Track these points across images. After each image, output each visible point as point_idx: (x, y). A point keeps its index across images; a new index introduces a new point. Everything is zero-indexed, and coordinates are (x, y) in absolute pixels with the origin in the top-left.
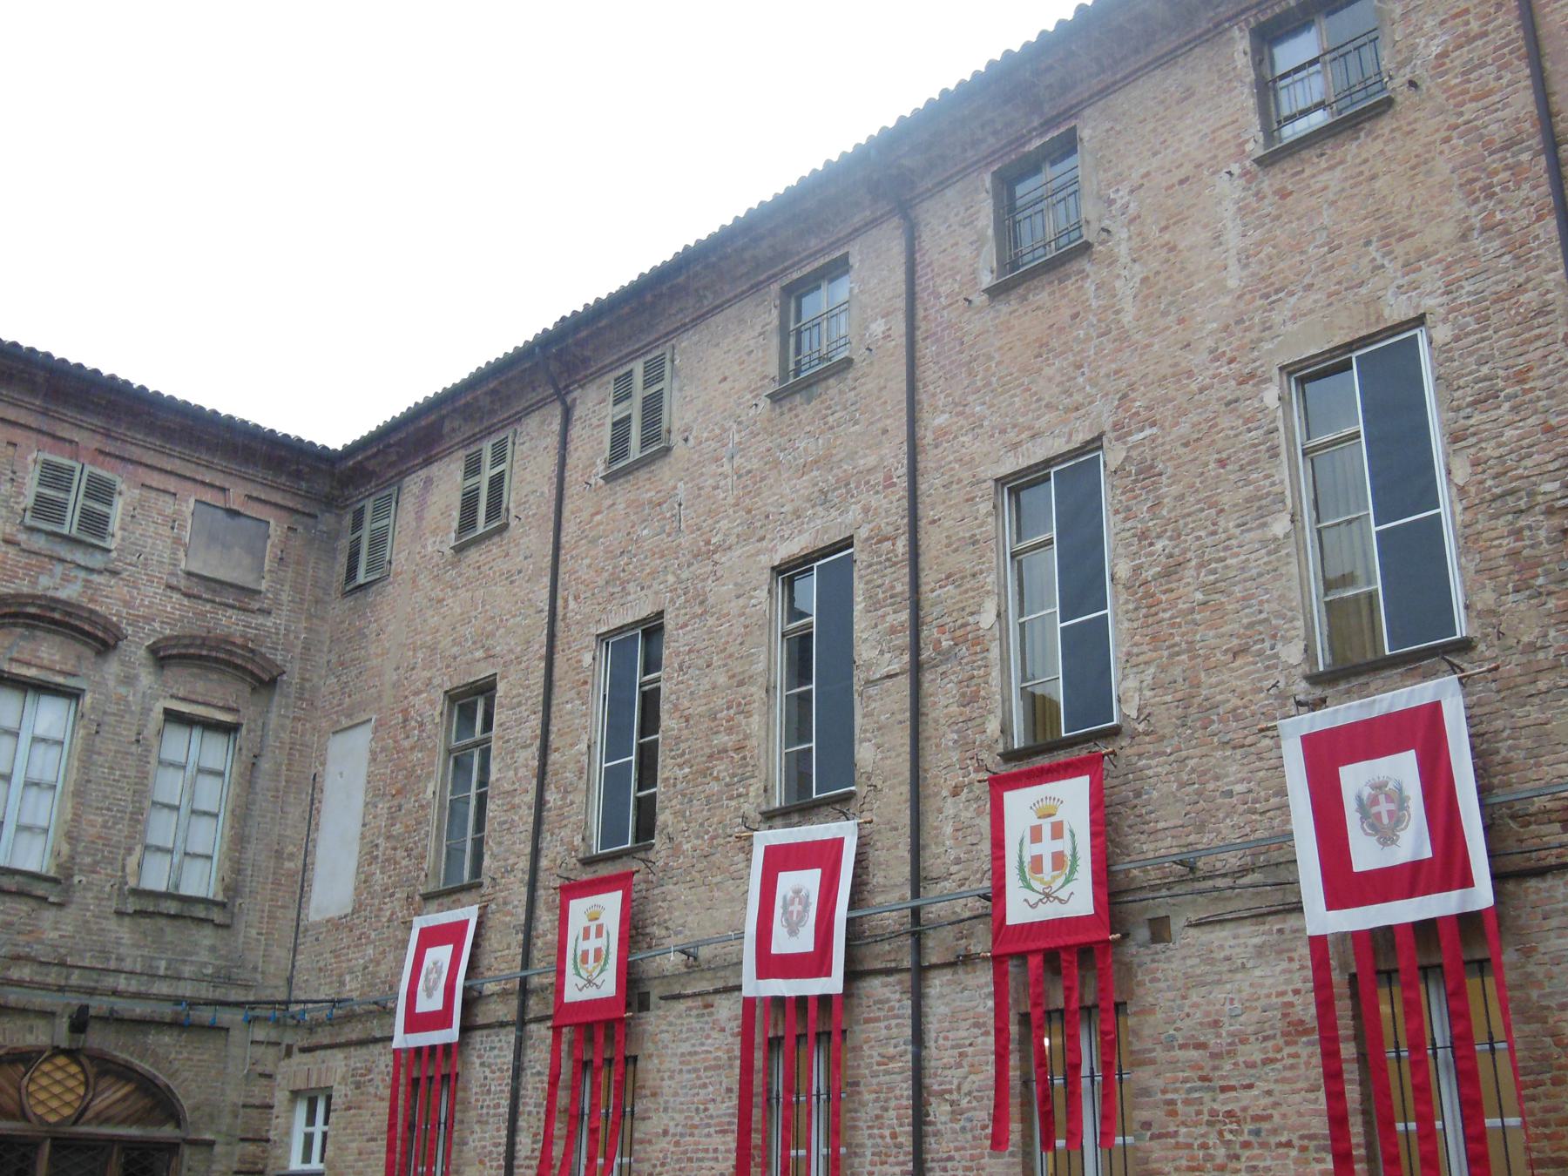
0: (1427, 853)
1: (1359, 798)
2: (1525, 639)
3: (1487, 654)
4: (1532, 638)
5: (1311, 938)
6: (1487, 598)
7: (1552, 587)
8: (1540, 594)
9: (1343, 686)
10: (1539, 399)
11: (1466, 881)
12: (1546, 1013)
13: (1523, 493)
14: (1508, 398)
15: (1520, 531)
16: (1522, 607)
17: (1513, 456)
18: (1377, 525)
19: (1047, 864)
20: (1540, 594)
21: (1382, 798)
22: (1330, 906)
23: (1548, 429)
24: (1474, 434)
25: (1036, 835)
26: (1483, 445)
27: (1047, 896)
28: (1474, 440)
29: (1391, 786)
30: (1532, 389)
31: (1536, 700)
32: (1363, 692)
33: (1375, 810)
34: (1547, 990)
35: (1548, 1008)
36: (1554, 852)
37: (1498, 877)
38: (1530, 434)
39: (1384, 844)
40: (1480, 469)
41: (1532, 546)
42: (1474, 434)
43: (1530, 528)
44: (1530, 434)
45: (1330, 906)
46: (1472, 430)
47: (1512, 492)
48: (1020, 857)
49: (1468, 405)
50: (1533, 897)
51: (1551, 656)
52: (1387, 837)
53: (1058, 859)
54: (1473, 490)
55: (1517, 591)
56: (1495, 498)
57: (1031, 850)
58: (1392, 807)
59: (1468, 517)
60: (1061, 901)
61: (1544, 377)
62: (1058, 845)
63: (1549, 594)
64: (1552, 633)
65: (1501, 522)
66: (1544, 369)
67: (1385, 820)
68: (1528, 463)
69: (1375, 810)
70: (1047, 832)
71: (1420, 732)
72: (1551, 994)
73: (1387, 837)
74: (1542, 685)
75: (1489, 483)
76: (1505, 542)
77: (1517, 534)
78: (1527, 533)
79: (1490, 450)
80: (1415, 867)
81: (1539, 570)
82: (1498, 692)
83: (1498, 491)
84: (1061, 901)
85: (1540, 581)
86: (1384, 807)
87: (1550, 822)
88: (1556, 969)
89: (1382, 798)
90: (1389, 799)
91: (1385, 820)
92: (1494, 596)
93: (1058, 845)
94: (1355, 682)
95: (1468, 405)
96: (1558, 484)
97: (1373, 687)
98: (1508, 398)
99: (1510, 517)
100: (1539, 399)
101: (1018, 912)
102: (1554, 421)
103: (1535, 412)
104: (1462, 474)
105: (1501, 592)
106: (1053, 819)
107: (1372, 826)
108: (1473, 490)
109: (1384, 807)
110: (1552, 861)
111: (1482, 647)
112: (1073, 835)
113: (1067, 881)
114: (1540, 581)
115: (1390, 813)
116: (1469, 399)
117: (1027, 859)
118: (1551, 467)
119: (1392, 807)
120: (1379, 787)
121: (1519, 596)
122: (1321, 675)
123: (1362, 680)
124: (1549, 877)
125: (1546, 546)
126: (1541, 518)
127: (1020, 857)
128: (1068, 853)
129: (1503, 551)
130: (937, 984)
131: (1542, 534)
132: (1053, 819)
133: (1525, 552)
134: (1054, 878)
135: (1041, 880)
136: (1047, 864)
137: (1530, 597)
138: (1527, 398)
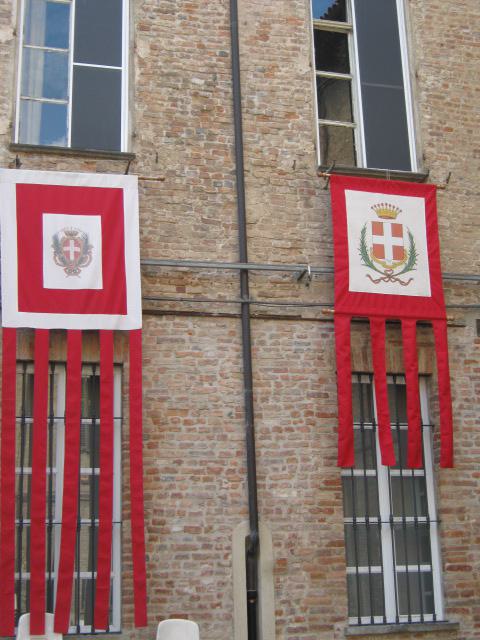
0: (99, 285)
1: (55, 238)
2: (170, 167)
3: (143, 169)
4: (174, 168)
5: (5, 329)
6: (147, 134)
7: (190, 141)
8: (182, 143)
9: (36, 159)
10: (199, 26)
11: (122, 310)
12: (150, 402)
13: (181, 79)
14: (180, 17)
15: (176, 100)
16: (170, 147)
17: (178, 53)
18: (75, 61)
19: (389, 253)
20: (182, 143)
21: (72, 242)
22: (22, 308)
23: (201, 46)
24: (155, 30)
25: (378, 229)
26: (160, 39)
27: (389, 277)
28: (155, 34)
29: (80, 235)
30: (196, 19)
31: (170, 206)
32: (51, 166)
33: (65, 249)
34: (153, 388)
35: (152, 399)
36: (169, 302)
37: (146, 313)
38: (191, 45)
39: (69, 273)
40: (156, 53)
41: (182, 113)
42: (155, 30)
43: (182, 101)
44: (191, 45)
45: (22, 308)
46: (153, 27)
47: (175, 75)
48: (363, 242)
49: (154, 11)
50: (152, 328)
51: (184, 183)
52: (72, 269)
53: (398, 252)
54: (149, 65)
55: (168, 136)
56: (163, 75)
57: (371, 240)
58: (78, 250)
59: (143, 80)
60: (402, 283)
61: (204, 14)
62: (398, 242)
63: (189, 144)
64: (187, 169)
65: (164, 90)
66: (204, 10)
67: (72, 258)
68: (188, 62)
69: (65, 249)
70: (387, 226)
71: (107, 205)
72: (154, 391)
73: (72, 269)
74: (176, 199)
75: (160, 64)
76: (165, 104)
77: (174, 101)
78: (179, 103)
79: (163, 42)
80: (90, 293)
81: (184, 129)
82: (147, 195)
83: (166, 71)
84: (402, 283)
85: (184, 135)
86: (72, 249)
87: (170, 284)
88: (161, 376)
89: (72, 242)
90: (77, 244)
91: (72, 258)
92: (154, 134)
93: (398, 242)
94: (45, 158)
95: (154, 11)
96: (203, 81)
97: (59, 166)
98: (180, 17)
99: (170, 89)
100: (199, 26)
101: (361, 280)
102: (206, 44)
103: (195, 33)
104: (143, 51)
105: (158, 133)
106: (393, 221)
107: (62, 259)
108: (149, 65)
109: (72, 249)
110: (167, 308)
111: (141, 164)
112: (410, 235)
113: (407, 269)
114: (184, 135)
115: (76, 254)
116: (155, 7)
117: (369, 246)
118: (200, 70)
119: (78, 250)
120: (71, 234)
121: (169, 140)
122: (16, 145)
123: (51, 159)
124: (164, 317)
125: (190, 115)
126: (190, 97)
127: (363, 242)
128: (407, 248)
129: (164, 108)
130: (264, 332)
131: (189, 108)
132: (393, 221)
133: (178, 115)
134: (395, 265)
135: (384, 265)
136: (389, 253)
137: (177, 143)
138: (192, 23)
